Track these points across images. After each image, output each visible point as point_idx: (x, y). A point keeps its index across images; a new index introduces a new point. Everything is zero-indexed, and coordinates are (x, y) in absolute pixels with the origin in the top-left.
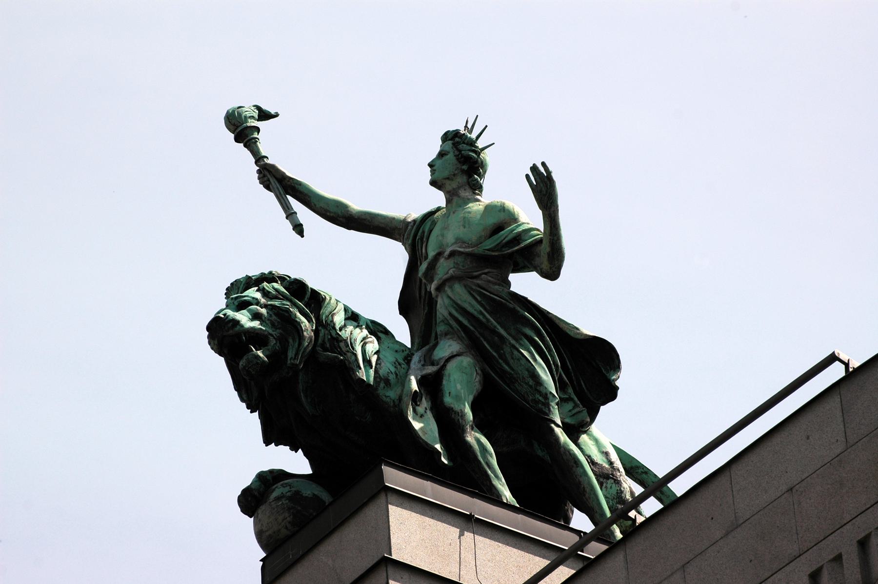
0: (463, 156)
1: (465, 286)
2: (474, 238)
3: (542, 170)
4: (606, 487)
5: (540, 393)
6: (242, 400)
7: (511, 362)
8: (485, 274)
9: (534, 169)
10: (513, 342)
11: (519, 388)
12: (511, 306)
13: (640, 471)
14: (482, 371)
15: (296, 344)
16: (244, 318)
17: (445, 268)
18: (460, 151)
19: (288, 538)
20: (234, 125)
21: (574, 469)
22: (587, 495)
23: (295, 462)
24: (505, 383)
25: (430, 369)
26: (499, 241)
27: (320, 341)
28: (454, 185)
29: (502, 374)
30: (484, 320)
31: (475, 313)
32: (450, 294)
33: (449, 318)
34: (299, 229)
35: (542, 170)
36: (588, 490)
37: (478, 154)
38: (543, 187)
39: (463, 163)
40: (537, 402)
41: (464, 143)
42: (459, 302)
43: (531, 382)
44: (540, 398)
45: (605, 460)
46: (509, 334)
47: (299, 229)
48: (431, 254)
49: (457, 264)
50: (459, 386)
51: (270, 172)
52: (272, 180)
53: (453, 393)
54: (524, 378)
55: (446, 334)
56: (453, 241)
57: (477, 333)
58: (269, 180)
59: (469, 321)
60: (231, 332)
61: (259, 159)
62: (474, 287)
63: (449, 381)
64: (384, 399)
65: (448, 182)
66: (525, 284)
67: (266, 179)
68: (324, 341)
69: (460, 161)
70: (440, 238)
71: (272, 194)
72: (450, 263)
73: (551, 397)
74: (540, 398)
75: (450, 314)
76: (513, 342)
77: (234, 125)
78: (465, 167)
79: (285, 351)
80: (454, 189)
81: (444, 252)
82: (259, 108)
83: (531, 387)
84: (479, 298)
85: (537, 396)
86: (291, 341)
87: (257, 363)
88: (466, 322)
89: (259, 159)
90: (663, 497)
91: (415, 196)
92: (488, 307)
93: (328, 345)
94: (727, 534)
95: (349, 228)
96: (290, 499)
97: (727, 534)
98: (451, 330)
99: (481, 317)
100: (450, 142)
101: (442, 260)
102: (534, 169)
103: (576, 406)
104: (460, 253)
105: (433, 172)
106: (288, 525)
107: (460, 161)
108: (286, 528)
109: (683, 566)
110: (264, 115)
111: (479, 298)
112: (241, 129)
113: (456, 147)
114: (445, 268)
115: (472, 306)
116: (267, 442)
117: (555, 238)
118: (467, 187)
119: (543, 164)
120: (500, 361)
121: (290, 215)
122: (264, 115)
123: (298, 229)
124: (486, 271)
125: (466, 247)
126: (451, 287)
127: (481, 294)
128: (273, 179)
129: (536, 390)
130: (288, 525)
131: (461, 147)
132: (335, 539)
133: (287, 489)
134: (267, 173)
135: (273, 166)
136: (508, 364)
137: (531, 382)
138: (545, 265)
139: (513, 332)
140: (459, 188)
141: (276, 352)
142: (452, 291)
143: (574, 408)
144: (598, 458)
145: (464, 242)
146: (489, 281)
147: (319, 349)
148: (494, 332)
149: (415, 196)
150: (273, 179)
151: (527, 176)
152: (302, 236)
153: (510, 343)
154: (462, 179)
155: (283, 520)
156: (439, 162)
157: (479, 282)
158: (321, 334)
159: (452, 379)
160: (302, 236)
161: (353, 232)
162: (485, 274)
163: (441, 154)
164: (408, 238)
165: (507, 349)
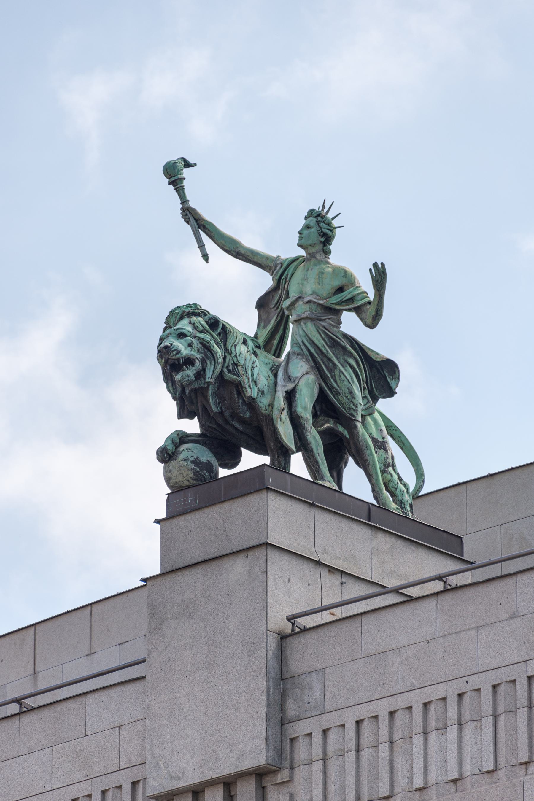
0: (322, 232)
1: (315, 325)
2: (325, 294)
3: (380, 266)
4: (379, 455)
5: (353, 403)
6: (169, 391)
7: (339, 382)
8: (329, 319)
9: (375, 265)
10: (342, 368)
11: (341, 399)
12: (343, 344)
13: (392, 429)
14: (319, 384)
15: (213, 367)
16: (180, 345)
17: (301, 309)
18: (321, 228)
19: (188, 487)
20: (170, 175)
21: (365, 451)
22: (370, 467)
23: (192, 426)
24: (332, 393)
25: (290, 386)
26: (341, 299)
27: (226, 365)
28: (314, 250)
29: (331, 388)
30: (325, 352)
31: (320, 346)
32: (304, 329)
33: (301, 344)
34: (206, 257)
35: (380, 266)
36: (371, 464)
37: (332, 231)
38: (379, 276)
39: (322, 236)
40: (350, 409)
41: (324, 222)
42: (310, 336)
43: (349, 397)
44: (353, 407)
45: (380, 436)
46: (339, 362)
47: (206, 257)
48: (293, 295)
49: (311, 309)
50: (306, 400)
51: (190, 213)
52: (192, 219)
53: (303, 405)
54: (345, 393)
55: (298, 355)
56: (310, 292)
57: (319, 360)
58: (189, 218)
59: (315, 350)
60: (174, 357)
61: (184, 201)
62: (321, 328)
63: (300, 394)
64: (260, 404)
65: (310, 247)
66: (350, 324)
67: (187, 217)
68: (228, 364)
69: (319, 230)
70: (301, 286)
71: (189, 227)
72: (307, 307)
73: (359, 405)
74: (353, 407)
75: (303, 342)
76: (342, 368)
77: (170, 175)
78: (323, 240)
79: (204, 370)
80: (313, 253)
81: (303, 298)
82: (184, 160)
83: (349, 399)
84: (323, 336)
85: (351, 405)
86: (208, 362)
87: (188, 380)
88: (313, 351)
89: (184, 201)
90: (403, 447)
91: (286, 247)
92: (328, 343)
93: (231, 368)
94: (510, 618)
95: (236, 257)
96: (193, 462)
97: (510, 618)
98: (302, 352)
99: (323, 349)
100: (315, 219)
101: (300, 302)
102: (375, 265)
103: (368, 402)
104: (315, 303)
105: (301, 238)
106: (190, 479)
107: (319, 230)
108: (188, 481)
109: (477, 627)
110: (188, 165)
111: (323, 336)
112: (174, 174)
113: (318, 224)
114: (301, 309)
115: (319, 341)
116: (179, 419)
117: (380, 308)
118: (322, 253)
119: (382, 264)
120: (332, 380)
121: (201, 246)
122: (188, 165)
123: (206, 257)
124: (329, 317)
125: (319, 299)
126: (305, 324)
127: (325, 333)
128: (190, 215)
129: (352, 401)
130: (190, 479)
131: (322, 225)
132: (226, 506)
133: (191, 454)
134: (188, 213)
135: (194, 210)
136: (336, 382)
137: (349, 397)
138: (369, 321)
139: (342, 361)
140: (317, 252)
141: (199, 370)
142: (306, 327)
143: (367, 403)
144: (375, 435)
145: (318, 296)
146: (331, 324)
147: (225, 370)
148: (330, 360)
149: (286, 247)
150: (190, 215)
151: (370, 270)
152: (207, 262)
153: (339, 369)
154: (320, 247)
155: (187, 476)
156: (306, 232)
157: (324, 324)
158: (227, 360)
159: (302, 393)
160: (207, 262)
161: (238, 260)
162: (329, 319)
163: (307, 227)
164: (276, 275)
165: (337, 373)
